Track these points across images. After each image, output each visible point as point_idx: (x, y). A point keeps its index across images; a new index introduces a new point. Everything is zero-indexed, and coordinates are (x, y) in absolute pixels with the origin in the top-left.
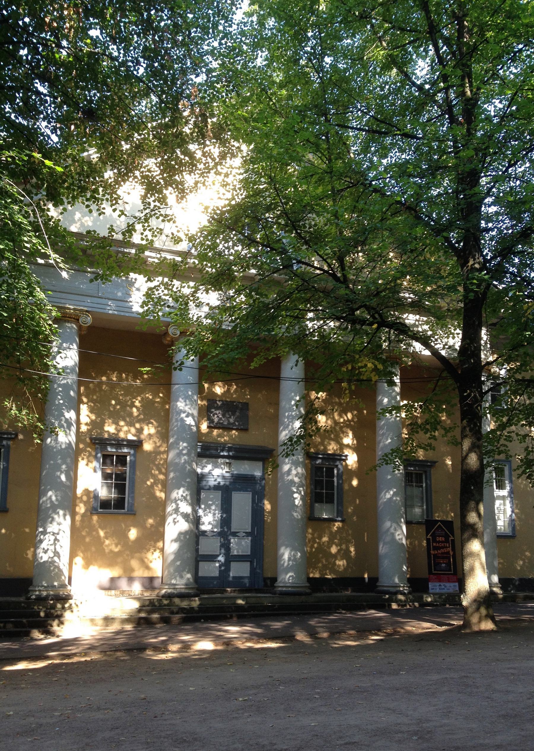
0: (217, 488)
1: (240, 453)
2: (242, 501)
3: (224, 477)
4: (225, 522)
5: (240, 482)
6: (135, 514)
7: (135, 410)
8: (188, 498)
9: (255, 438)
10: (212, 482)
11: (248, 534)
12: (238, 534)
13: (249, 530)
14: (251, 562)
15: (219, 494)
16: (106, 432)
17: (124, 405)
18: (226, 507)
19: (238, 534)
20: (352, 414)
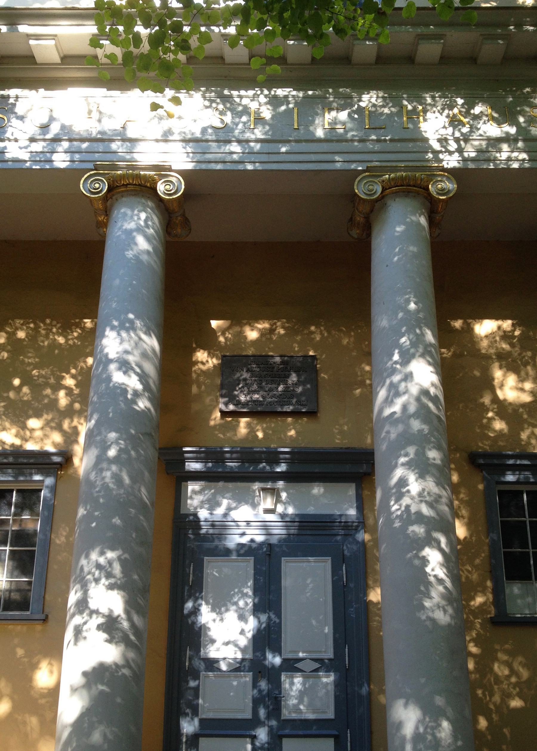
0: (247, 550)
1: (308, 467)
2: (308, 581)
3: (265, 527)
4: (266, 639)
5: (310, 534)
6: (45, 620)
7: (62, 393)
8: (117, 569)
9: (332, 433)
10: (234, 540)
11: (324, 665)
12: (299, 665)
13: (330, 655)
14: (337, 738)
15: (248, 566)
16: (97, 135)
17: (37, 388)
18: (268, 599)
19: (299, 665)
20: (348, 426)
